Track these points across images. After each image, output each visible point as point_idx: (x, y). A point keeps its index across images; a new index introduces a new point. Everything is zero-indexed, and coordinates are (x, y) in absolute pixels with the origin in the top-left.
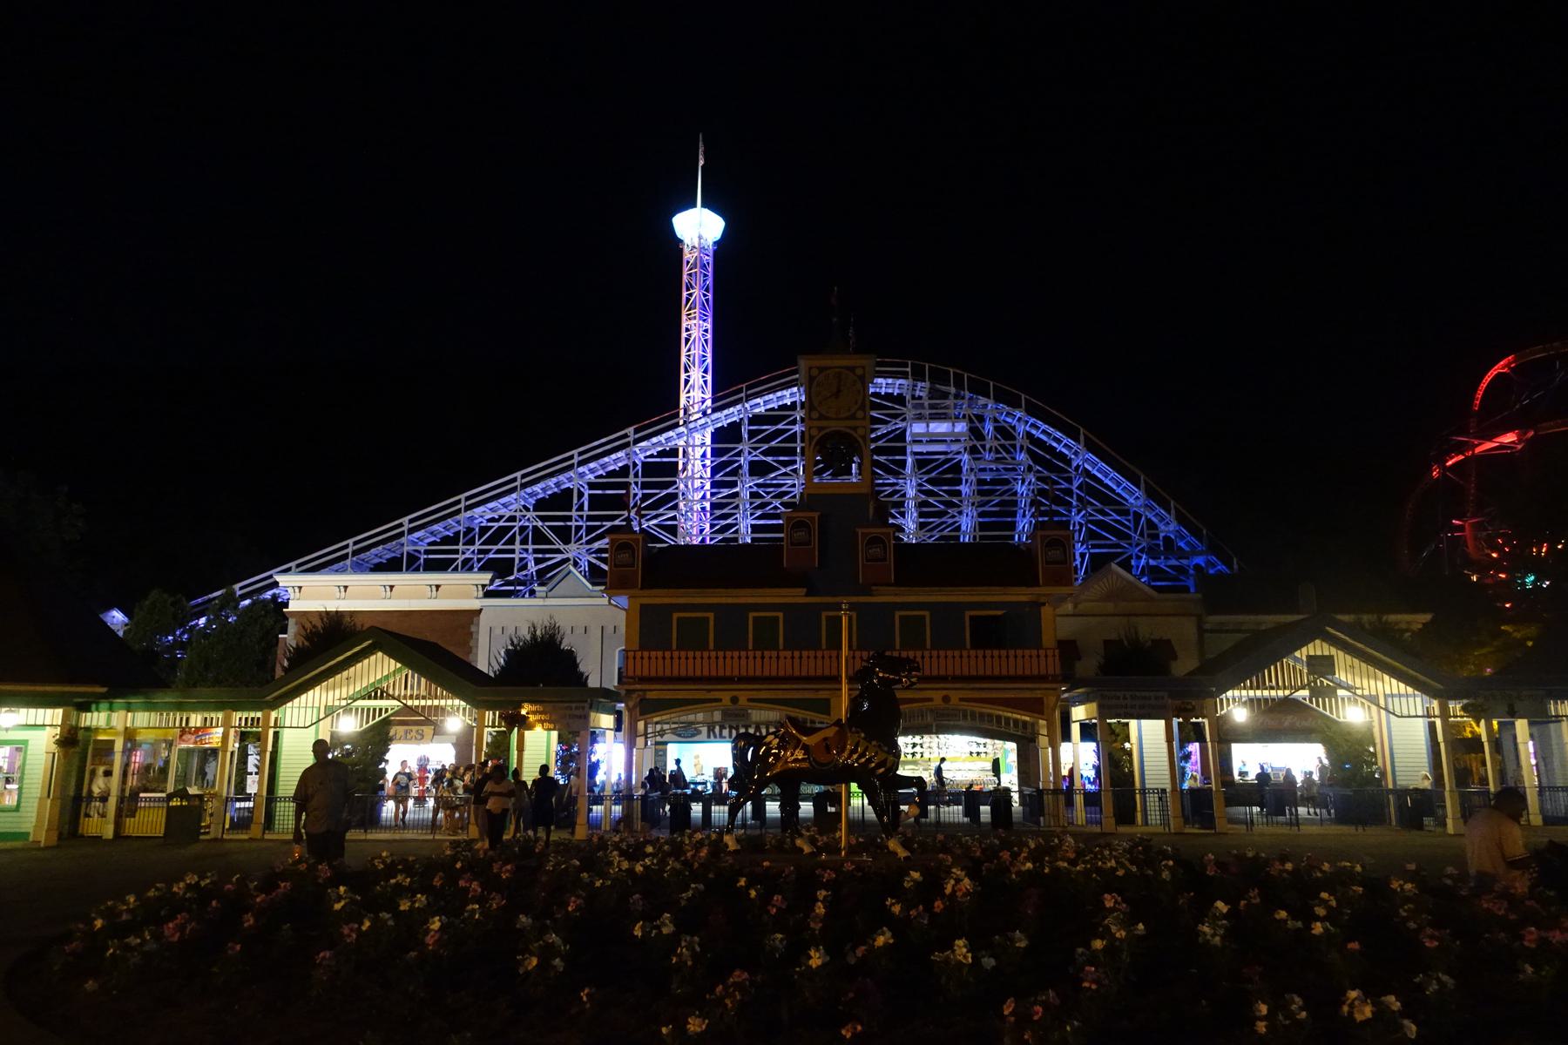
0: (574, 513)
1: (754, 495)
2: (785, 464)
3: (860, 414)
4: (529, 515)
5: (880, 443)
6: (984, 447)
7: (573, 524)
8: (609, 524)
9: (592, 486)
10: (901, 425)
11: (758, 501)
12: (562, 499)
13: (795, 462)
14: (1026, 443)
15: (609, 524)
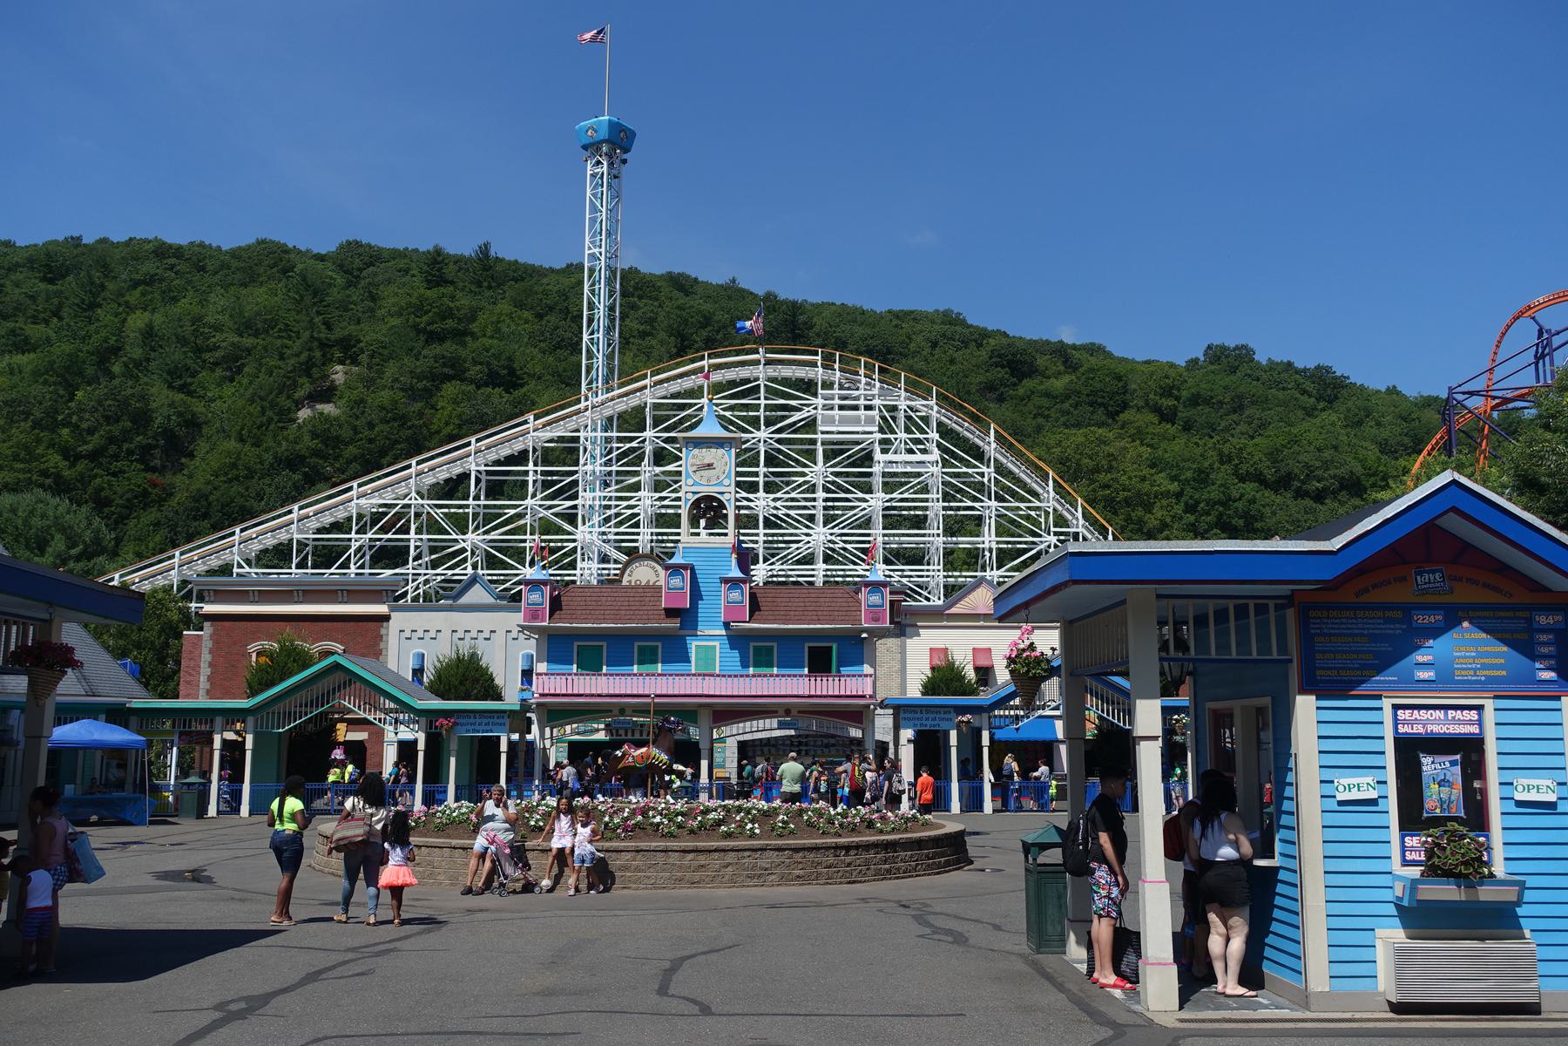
8: (622, 529)
12: (454, 487)
15: (622, 529)
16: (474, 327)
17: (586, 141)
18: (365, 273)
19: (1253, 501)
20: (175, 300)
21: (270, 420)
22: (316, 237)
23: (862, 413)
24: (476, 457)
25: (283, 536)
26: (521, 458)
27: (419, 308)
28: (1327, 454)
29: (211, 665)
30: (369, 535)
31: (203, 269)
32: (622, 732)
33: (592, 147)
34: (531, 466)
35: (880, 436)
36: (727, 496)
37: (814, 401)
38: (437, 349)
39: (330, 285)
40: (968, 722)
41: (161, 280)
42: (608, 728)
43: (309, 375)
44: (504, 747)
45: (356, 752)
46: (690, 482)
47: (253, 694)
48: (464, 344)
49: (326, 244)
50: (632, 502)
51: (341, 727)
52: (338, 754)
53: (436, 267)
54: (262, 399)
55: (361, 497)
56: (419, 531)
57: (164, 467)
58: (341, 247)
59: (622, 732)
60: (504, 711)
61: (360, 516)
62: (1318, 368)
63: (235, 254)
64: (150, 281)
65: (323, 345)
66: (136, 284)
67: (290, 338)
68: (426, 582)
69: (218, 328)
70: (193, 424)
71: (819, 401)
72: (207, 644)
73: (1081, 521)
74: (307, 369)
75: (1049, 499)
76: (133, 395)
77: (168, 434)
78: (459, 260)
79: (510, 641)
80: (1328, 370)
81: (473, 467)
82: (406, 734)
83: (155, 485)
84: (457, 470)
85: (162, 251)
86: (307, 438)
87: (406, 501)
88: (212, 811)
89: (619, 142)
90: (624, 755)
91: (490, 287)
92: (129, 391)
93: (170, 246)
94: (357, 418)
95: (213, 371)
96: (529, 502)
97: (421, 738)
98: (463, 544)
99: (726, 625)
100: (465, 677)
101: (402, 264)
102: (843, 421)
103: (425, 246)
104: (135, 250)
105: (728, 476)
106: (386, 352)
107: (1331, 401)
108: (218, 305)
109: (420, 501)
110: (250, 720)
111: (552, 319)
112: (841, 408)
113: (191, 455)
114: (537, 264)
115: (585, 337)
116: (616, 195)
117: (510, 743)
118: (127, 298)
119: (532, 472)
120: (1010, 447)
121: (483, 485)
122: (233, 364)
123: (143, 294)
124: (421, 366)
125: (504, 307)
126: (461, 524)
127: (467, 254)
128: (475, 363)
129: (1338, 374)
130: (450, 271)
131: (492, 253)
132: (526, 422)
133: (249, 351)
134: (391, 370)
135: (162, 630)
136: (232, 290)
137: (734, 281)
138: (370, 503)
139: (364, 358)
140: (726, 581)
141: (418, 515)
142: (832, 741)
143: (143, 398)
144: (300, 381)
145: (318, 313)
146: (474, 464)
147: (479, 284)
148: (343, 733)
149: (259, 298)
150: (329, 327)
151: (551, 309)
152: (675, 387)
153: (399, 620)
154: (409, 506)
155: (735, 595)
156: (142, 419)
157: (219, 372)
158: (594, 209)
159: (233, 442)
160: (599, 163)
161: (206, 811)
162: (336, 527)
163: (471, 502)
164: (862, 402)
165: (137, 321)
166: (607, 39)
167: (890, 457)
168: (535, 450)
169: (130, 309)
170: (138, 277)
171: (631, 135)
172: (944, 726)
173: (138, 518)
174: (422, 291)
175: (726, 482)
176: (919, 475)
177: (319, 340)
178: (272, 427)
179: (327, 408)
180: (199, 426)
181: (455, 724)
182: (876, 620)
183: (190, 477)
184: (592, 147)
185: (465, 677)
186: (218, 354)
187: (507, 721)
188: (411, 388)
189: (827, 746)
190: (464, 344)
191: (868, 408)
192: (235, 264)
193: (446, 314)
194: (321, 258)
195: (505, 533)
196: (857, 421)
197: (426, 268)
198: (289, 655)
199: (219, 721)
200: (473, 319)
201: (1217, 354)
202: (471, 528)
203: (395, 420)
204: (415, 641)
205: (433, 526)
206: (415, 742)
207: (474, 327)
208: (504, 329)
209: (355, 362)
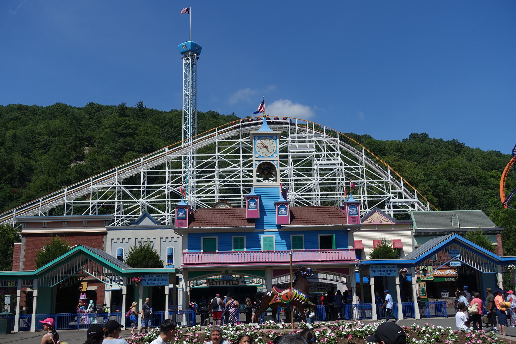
8: (208, 195)
12: (135, 179)
15: (208, 195)
16: (138, 132)
17: (182, 51)
19: (446, 186)
20: (25, 125)
21: (60, 167)
22: (78, 101)
23: (308, 144)
24: (143, 166)
25: (60, 202)
26: (163, 166)
27: (117, 125)
28: (464, 170)
29: (25, 257)
30: (98, 201)
31: (36, 114)
32: (214, 283)
33: (185, 53)
34: (167, 169)
35: (315, 153)
36: (275, 162)
37: (287, 139)
38: (122, 140)
39: (83, 118)
40: (406, 272)
41: (20, 118)
42: (208, 282)
43: (75, 151)
44: (167, 292)
45: (92, 295)
46: (257, 155)
47: (39, 266)
48: (134, 138)
49: (82, 104)
50: (210, 184)
51: (85, 284)
52: (83, 297)
53: (123, 110)
54: (57, 160)
55: (94, 185)
56: (119, 199)
57: (19, 186)
58: (87, 105)
59: (214, 283)
60: (167, 273)
61: (94, 193)
62: (453, 140)
63: (47, 108)
64: (16, 119)
65: (81, 139)
66: (11, 120)
67: (68, 137)
68: (122, 221)
69: (40, 134)
70: (31, 170)
71: (289, 139)
72: (23, 247)
73: (403, 187)
74: (74, 148)
75: (388, 178)
76: (7, 159)
77: (21, 173)
78: (131, 109)
79: (162, 242)
80: (457, 141)
81: (142, 170)
82: (116, 286)
83: (14, 192)
84: (135, 172)
85: (20, 108)
86: (74, 173)
87: (113, 186)
88: (16, 329)
89: (195, 51)
90: (273, 295)
91: (143, 118)
92: (6, 157)
93: (24, 106)
94: (93, 165)
95: (39, 150)
96: (166, 184)
97: (124, 289)
98: (138, 204)
99: (278, 226)
100: (145, 256)
101: (110, 110)
102: (300, 147)
103: (117, 103)
104: (10, 108)
105: (276, 152)
106: (104, 141)
107: (459, 152)
108: (41, 126)
109: (119, 185)
110: (36, 281)
111: (167, 128)
112: (299, 142)
113: (30, 181)
114: (160, 110)
115: (183, 126)
116: (195, 72)
117: (170, 290)
118: (7, 125)
120: (372, 158)
121: (146, 178)
122: (46, 147)
123: (13, 124)
124: (118, 145)
125: (149, 124)
126: (137, 195)
127: (134, 106)
128: (138, 144)
129: (461, 143)
130: (128, 112)
131: (144, 107)
132: (164, 151)
133: (52, 142)
134: (106, 148)
135: (6, 243)
136: (46, 121)
137: (233, 114)
138: (98, 187)
139: (96, 144)
140: (277, 204)
141: (119, 192)
143: (11, 160)
144: (72, 153)
145: (79, 128)
146: (142, 170)
147: (139, 117)
148: (85, 287)
149: (56, 124)
150: (83, 133)
151: (166, 125)
152: (227, 135)
153: (111, 234)
154: (114, 188)
155: (283, 211)
156: (11, 168)
157: (41, 151)
158: (186, 77)
159: (45, 176)
160: (188, 59)
161: (13, 330)
162: (85, 197)
163: (141, 185)
164: (307, 139)
165: (10, 133)
166: (190, 12)
167: (320, 162)
168: (168, 163)
169: (7, 129)
170: (11, 117)
171: (200, 48)
172: (393, 274)
173: (8, 205)
174: (117, 118)
175: (275, 155)
176: (332, 170)
177: (79, 137)
178: (61, 170)
179: (83, 163)
180: (33, 170)
181: (142, 280)
182: (354, 221)
183: (29, 189)
184: (185, 53)
185: (145, 256)
186: (41, 143)
187: (168, 278)
188: (114, 154)
190: (134, 138)
191: (310, 141)
192: (47, 112)
193: (128, 127)
194: (80, 109)
195: (157, 198)
196: (306, 147)
197: (119, 111)
198: (57, 248)
199: (20, 282)
200: (137, 129)
201: (414, 137)
202: (141, 197)
203: (107, 165)
204: (119, 243)
205: (125, 196)
206: (121, 290)
207: (138, 132)
208: (149, 132)
209: (92, 146)
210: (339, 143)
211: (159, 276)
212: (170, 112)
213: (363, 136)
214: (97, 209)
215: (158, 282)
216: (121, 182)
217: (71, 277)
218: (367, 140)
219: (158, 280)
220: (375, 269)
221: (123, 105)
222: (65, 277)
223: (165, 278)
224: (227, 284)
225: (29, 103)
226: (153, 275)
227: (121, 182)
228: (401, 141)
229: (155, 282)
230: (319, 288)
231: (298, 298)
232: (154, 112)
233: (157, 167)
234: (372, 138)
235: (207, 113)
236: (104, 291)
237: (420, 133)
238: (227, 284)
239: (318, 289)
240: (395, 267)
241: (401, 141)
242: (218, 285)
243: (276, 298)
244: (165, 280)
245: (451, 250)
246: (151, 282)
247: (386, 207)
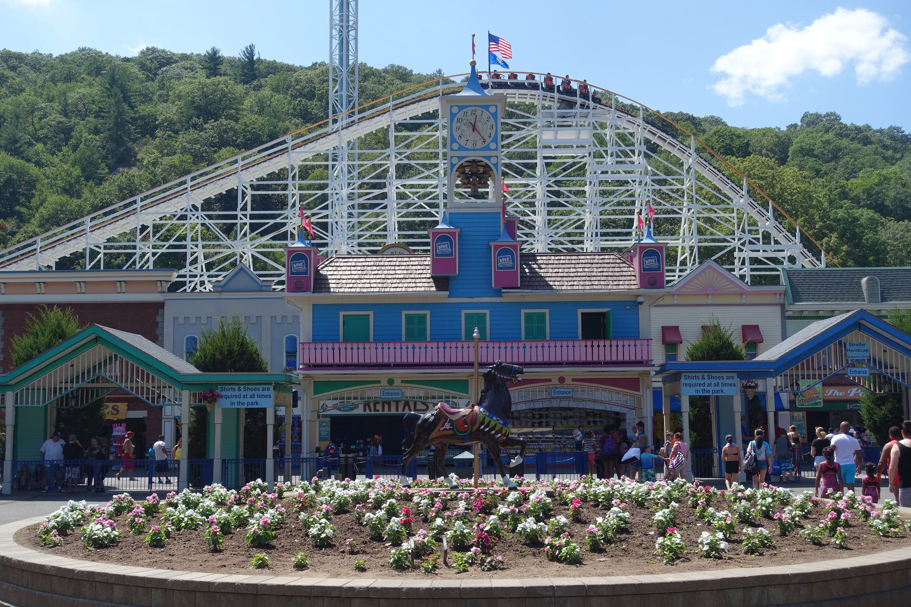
0: (248, 221)
1: (401, 196)
2: (426, 167)
3: (493, 146)
4: (197, 214)
5: (512, 149)
6: (606, 152)
7: (239, 221)
8: (272, 222)
9: (253, 187)
10: (535, 132)
11: (404, 202)
12: (228, 200)
13: (436, 166)
14: (644, 148)
15: (272, 222)
18: (160, 72)
24: (243, 174)
49: (134, 52)
53: (213, 62)
59: (379, 407)
63: (62, 59)
78: (232, 62)
80: (898, 130)
101: (187, 64)
103: (201, 49)
119: (293, 193)
127: (237, 56)
129: (906, 133)
137: (440, 72)
138: (149, 218)
142: (570, 413)
149: (78, 92)
189: (565, 418)
194: (126, 60)
210: (640, 132)
211: (255, 389)
212: (309, 68)
213: (706, 120)
214: (152, 259)
215: (253, 400)
216: (199, 206)
217: (78, 390)
218: (714, 129)
219: (251, 397)
220: (693, 381)
221: (215, 52)
222: (66, 388)
223: (266, 393)
224: (403, 410)
225: (26, 48)
226: (242, 387)
227: (199, 206)
228: (784, 128)
229: (246, 400)
230: (590, 419)
231: (487, 426)
232: (274, 68)
233: (271, 176)
234: (724, 124)
235: (385, 71)
236: (161, 419)
237: (823, 113)
238: (403, 410)
239: (589, 422)
240: (733, 378)
241: (784, 128)
242: (386, 412)
243: (443, 425)
244: (266, 396)
245: (851, 345)
246: (702, 388)
247: (736, 261)
